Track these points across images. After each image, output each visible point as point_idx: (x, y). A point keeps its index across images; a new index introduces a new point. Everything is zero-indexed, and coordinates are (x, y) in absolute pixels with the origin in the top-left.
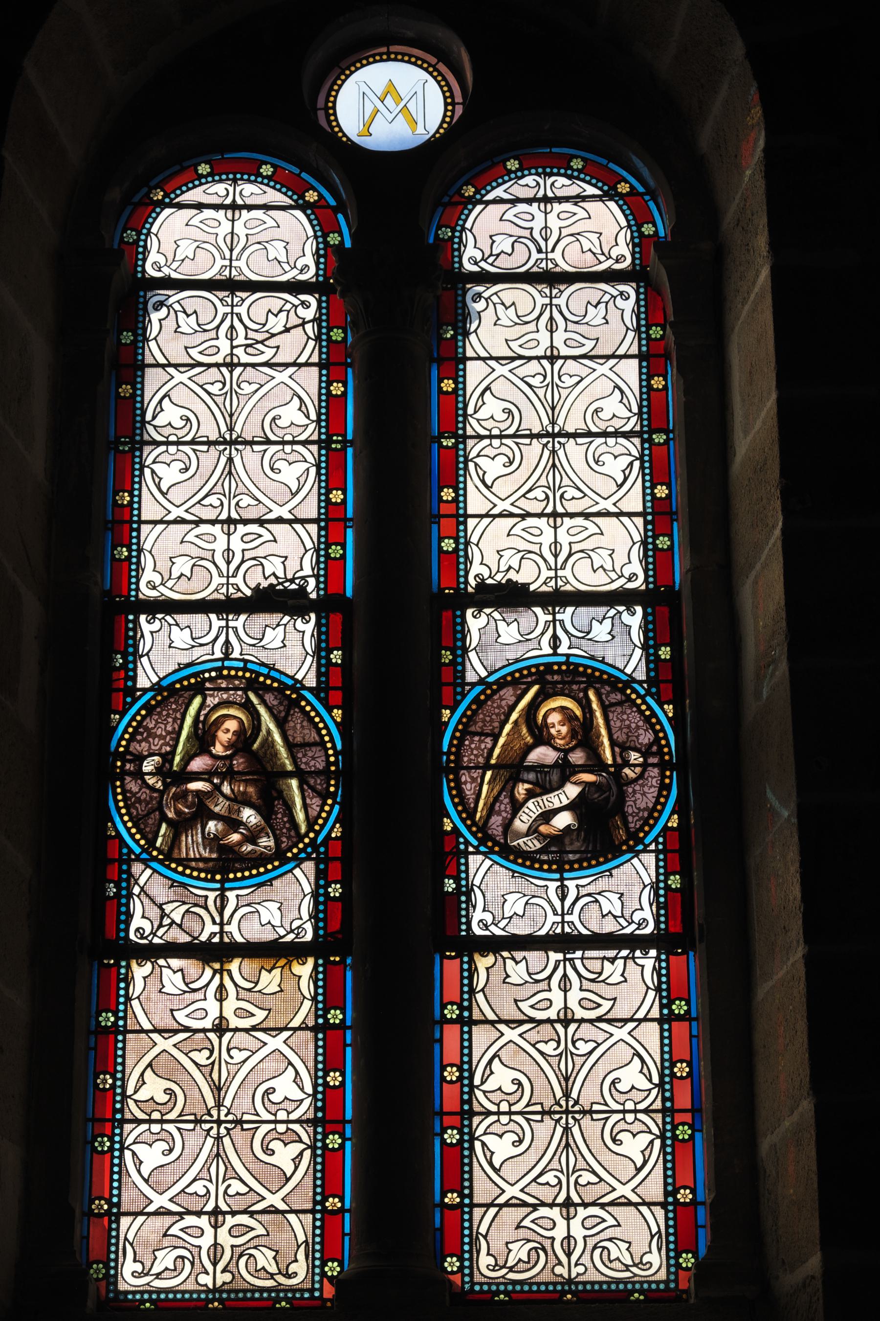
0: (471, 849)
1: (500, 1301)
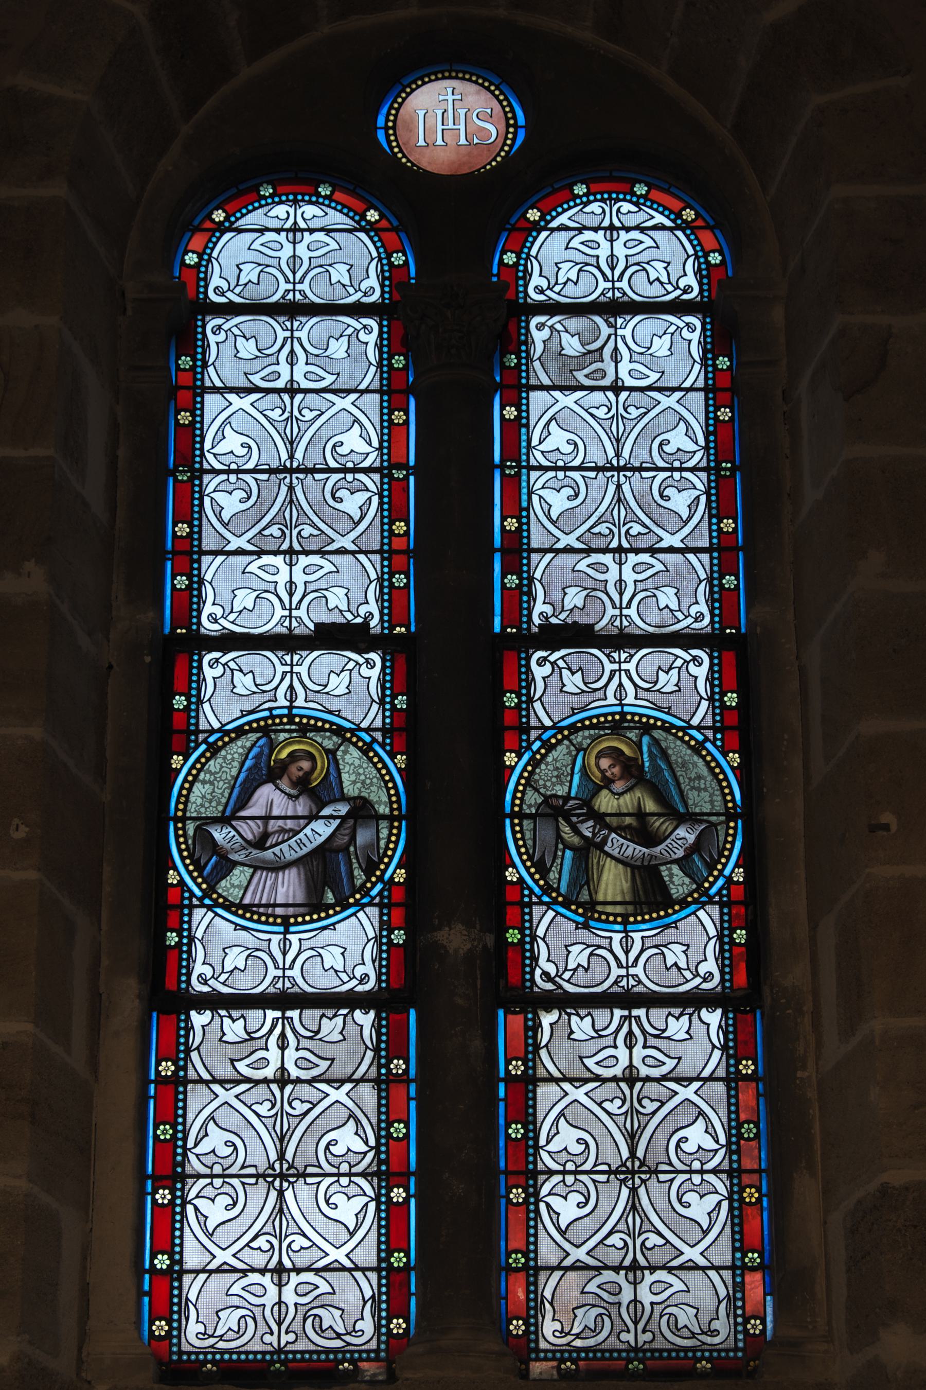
0: (534, 899)
1: (345, 1369)
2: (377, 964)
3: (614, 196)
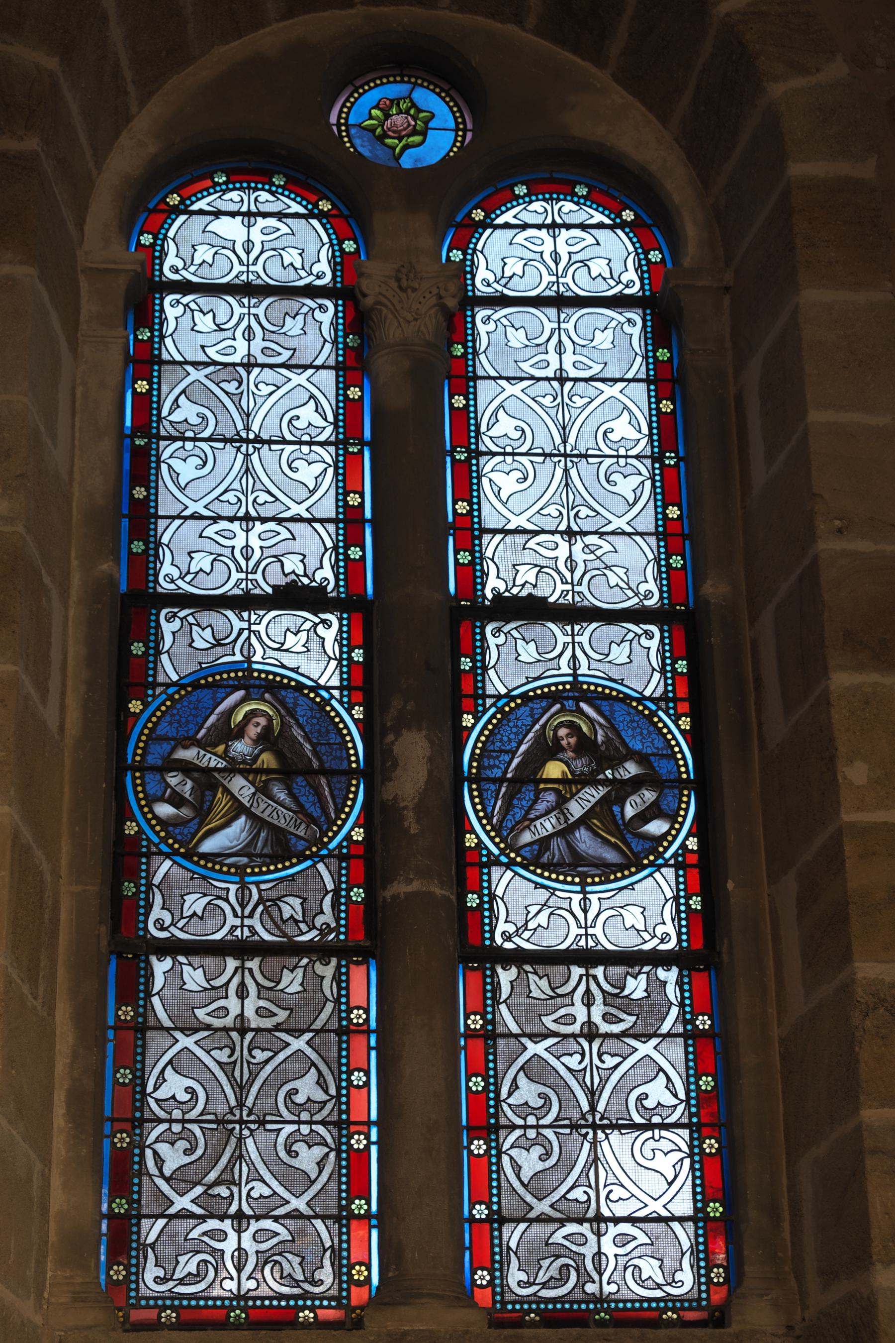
2: (676, 923)
3: (555, 196)
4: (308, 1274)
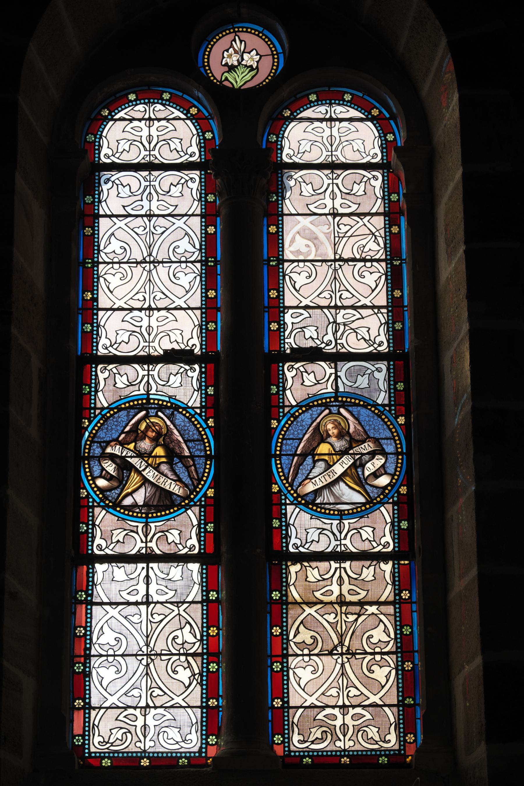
0: (288, 502)
4: (383, 737)
